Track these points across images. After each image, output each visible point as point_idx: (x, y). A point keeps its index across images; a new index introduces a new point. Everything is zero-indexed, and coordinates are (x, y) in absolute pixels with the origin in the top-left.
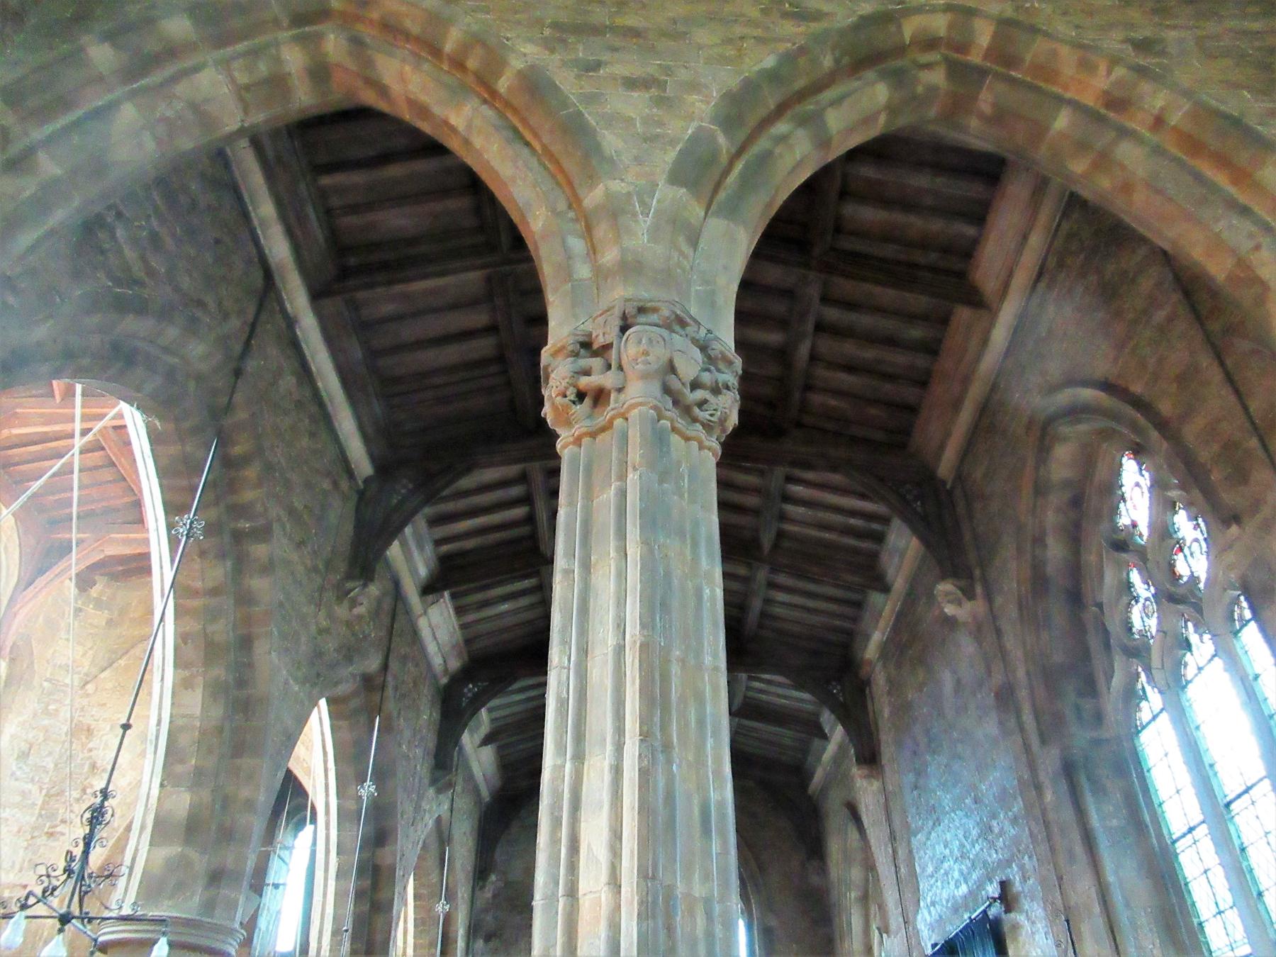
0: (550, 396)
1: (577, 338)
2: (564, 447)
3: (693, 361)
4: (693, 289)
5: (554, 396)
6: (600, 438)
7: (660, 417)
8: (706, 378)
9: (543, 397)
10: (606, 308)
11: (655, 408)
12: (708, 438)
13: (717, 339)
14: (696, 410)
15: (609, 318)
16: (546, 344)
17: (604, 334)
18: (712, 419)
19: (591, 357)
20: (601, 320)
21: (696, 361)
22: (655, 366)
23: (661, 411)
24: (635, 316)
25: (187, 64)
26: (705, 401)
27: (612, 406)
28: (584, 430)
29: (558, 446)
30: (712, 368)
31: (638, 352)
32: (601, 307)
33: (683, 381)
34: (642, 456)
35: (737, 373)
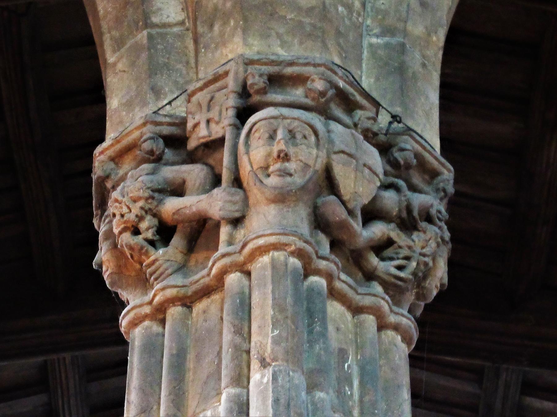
0: (109, 234)
1: (158, 129)
2: (134, 324)
3: (367, 171)
4: (365, 43)
5: (116, 231)
6: (199, 307)
7: (308, 271)
8: (389, 198)
9: (97, 234)
10: (210, 77)
11: (299, 254)
12: (395, 309)
13: (409, 130)
14: (374, 260)
15: (217, 95)
16: (103, 140)
17: (208, 121)
18: (402, 274)
19: (184, 162)
20: (202, 97)
21: (370, 169)
22: (298, 180)
23: (310, 258)
24: (263, 91)
25: (393, 280)
26: (389, 243)
27: (223, 248)
28: (170, 293)
29: (124, 322)
30: (401, 183)
31: (269, 155)
32: (201, 75)
33: (350, 206)
34: (276, 341)
35: (444, 190)
